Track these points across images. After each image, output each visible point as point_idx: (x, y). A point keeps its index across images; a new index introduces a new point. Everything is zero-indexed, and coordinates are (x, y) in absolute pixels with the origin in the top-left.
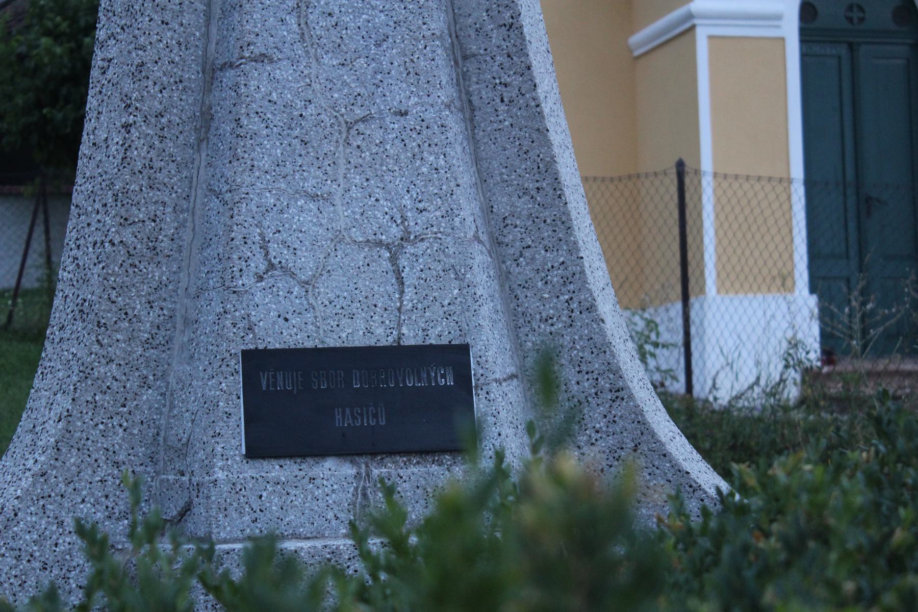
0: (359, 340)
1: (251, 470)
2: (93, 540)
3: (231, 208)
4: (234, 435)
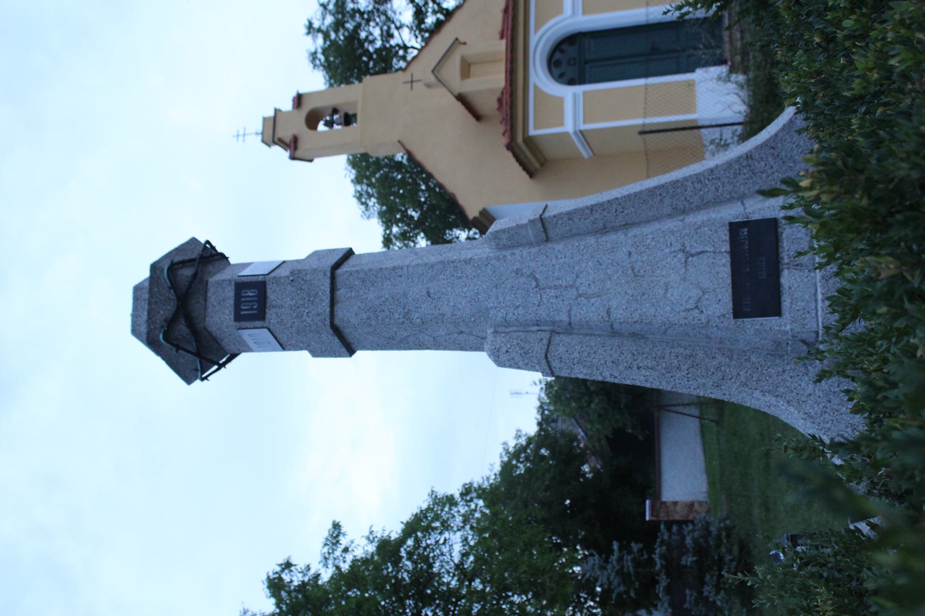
0: (728, 269)
1: (786, 314)
2: (822, 376)
3: (671, 325)
4: (774, 320)
